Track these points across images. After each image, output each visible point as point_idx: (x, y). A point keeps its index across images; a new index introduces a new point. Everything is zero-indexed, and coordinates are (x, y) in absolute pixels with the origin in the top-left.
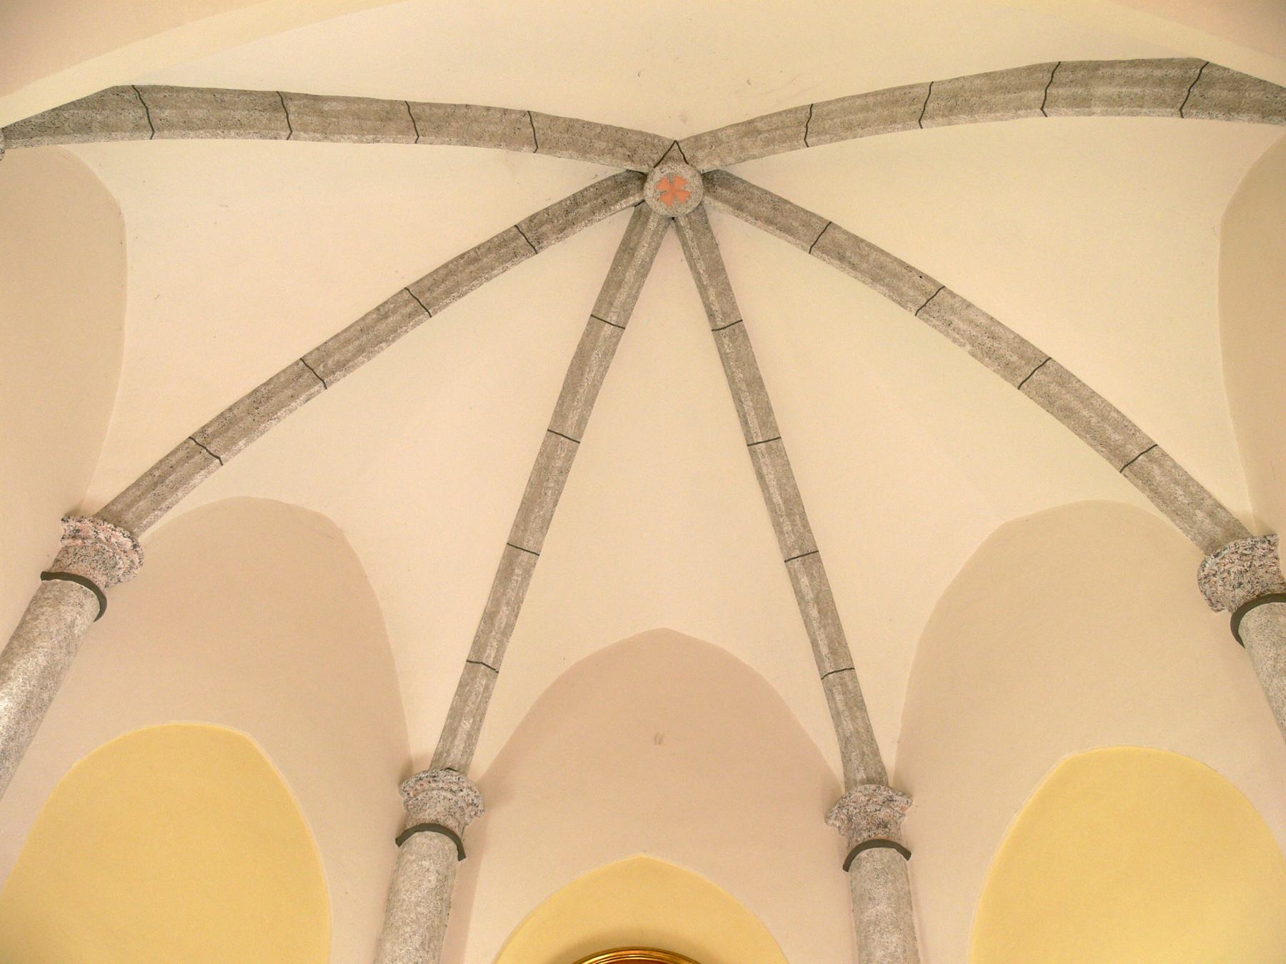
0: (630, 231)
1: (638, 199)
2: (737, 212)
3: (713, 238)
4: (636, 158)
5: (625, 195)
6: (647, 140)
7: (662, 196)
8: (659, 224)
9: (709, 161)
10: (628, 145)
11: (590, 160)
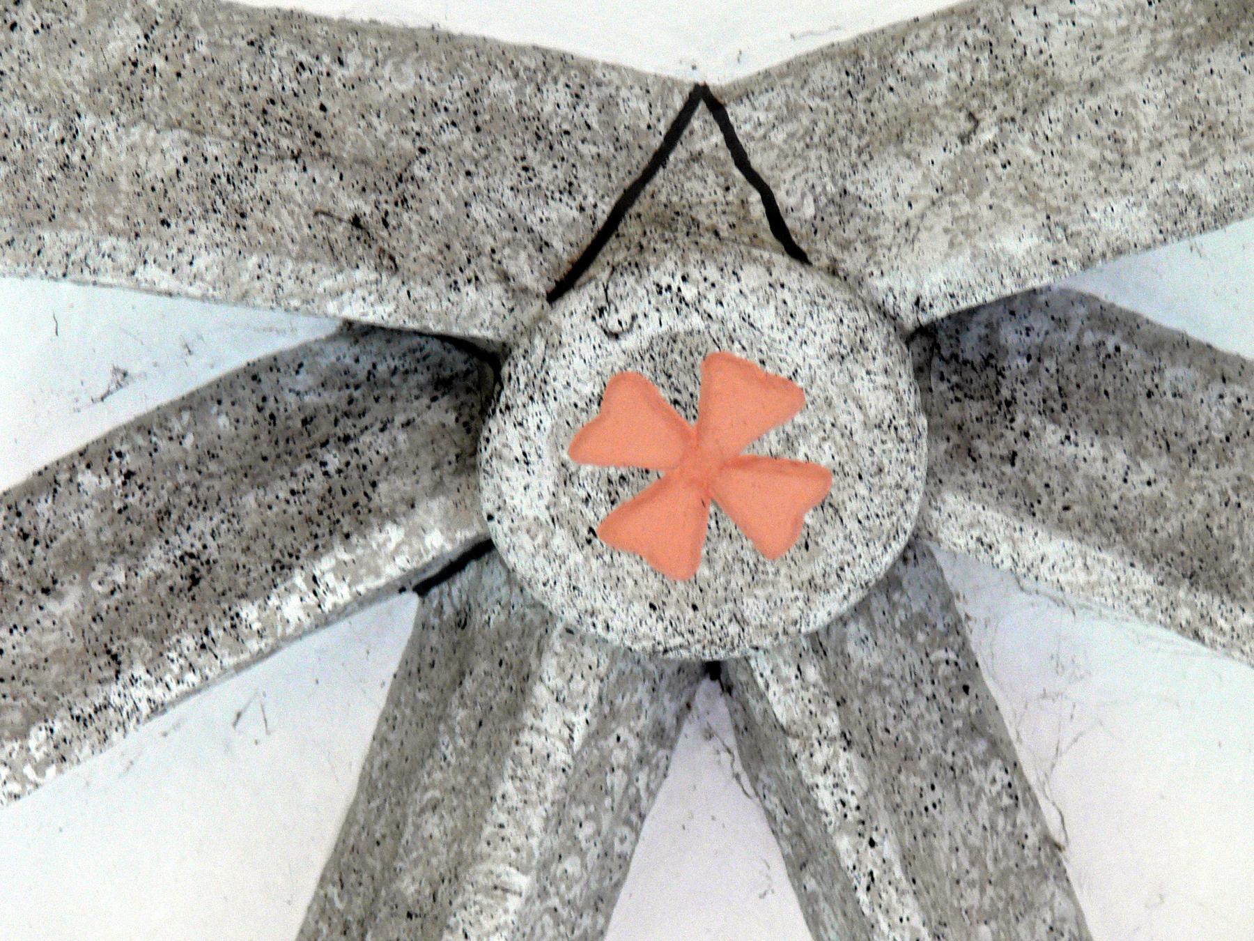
0: (391, 779)
1: (439, 542)
2: (1191, 602)
3: (1019, 795)
4: (412, 235)
5: (345, 513)
6: (497, 97)
7: (618, 509)
8: (607, 716)
9: (961, 233)
10: (353, 137)
11: (72, 268)
